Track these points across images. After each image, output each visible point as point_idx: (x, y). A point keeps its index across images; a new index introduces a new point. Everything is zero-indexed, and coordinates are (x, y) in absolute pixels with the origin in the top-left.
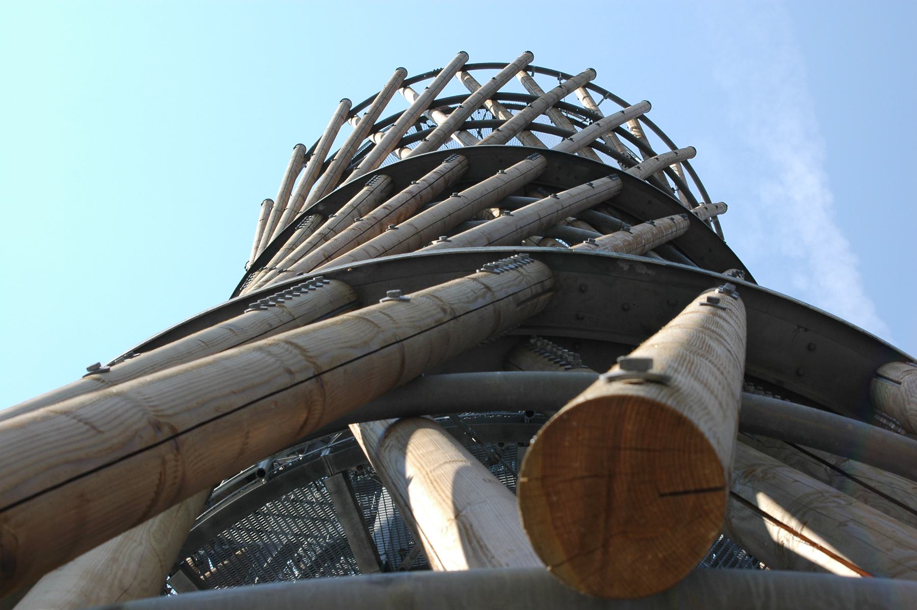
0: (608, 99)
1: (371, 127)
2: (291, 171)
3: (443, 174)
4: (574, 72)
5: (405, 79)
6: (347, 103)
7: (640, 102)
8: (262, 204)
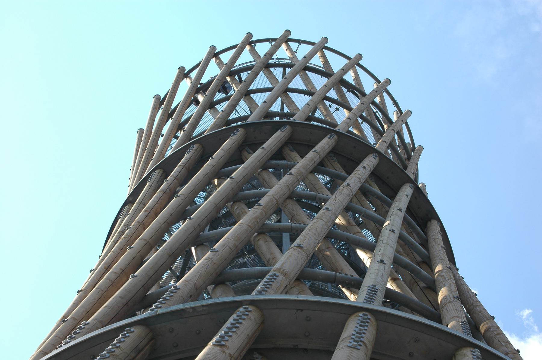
0: (302, 44)
1: (168, 114)
2: (137, 149)
3: (184, 165)
4: (278, 35)
5: (185, 73)
6: (158, 98)
7: (319, 41)
8: (131, 170)
